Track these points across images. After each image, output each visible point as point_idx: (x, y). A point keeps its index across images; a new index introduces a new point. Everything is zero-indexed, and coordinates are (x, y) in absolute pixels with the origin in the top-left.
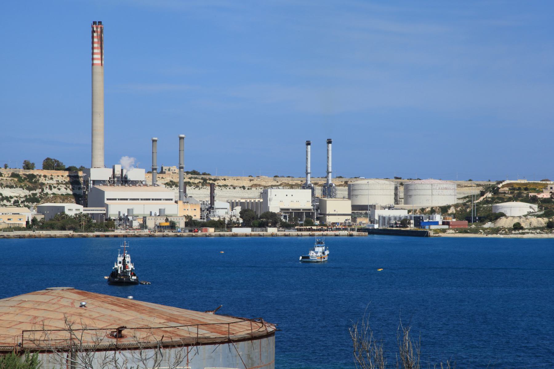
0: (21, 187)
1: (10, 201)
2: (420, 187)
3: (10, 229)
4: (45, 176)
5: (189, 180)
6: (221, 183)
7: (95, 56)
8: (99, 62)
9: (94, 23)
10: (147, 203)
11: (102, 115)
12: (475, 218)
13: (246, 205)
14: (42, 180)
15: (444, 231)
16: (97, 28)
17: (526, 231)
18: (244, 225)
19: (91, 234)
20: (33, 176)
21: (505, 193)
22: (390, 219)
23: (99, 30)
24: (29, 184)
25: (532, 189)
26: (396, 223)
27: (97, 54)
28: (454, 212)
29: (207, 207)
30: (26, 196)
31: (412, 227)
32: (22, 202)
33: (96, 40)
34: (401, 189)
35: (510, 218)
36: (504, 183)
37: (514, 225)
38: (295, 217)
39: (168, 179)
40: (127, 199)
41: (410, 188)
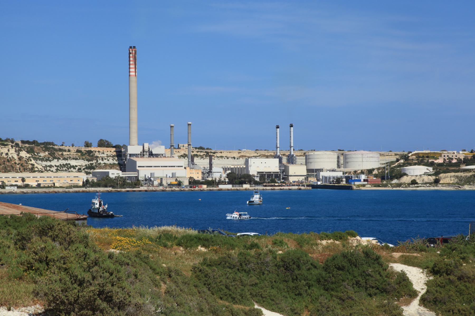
0: (83, 159)
1: (75, 169)
2: (354, 156)
3: (70, 187)
4: (99, 152)
5: (197, 153)
6: (219, 155)
7: (131, 70)
8: (134, 74)
9: (131, 47)
10: (164, 169)
11: (136, 110)
12: (387, 177)
13: (234, 169)
14: (97, 154)
15: (364, 186)
16: (132, 50)
17: (420, 185)
18: (229, 183)
19: (123, 190)
20: (90, 152)
21: (413, 160)
22: (330, 178)
23: (134, 52)
24: (88, 157)
25: (431, 157)
26: (333, 181)
27: (132, 68)
28: (377, 173)
29: (207, 171)
30: (86, 165)
31: (344, 183)
32: (83, 169)
33: (131, 59)
34: (342, 158)
35: (409, 177)
36: (413, 153)
37: (412, 181)
38: (266, 178)
39: (182, 153)
40: (152, 167)
41: (348, 157)
